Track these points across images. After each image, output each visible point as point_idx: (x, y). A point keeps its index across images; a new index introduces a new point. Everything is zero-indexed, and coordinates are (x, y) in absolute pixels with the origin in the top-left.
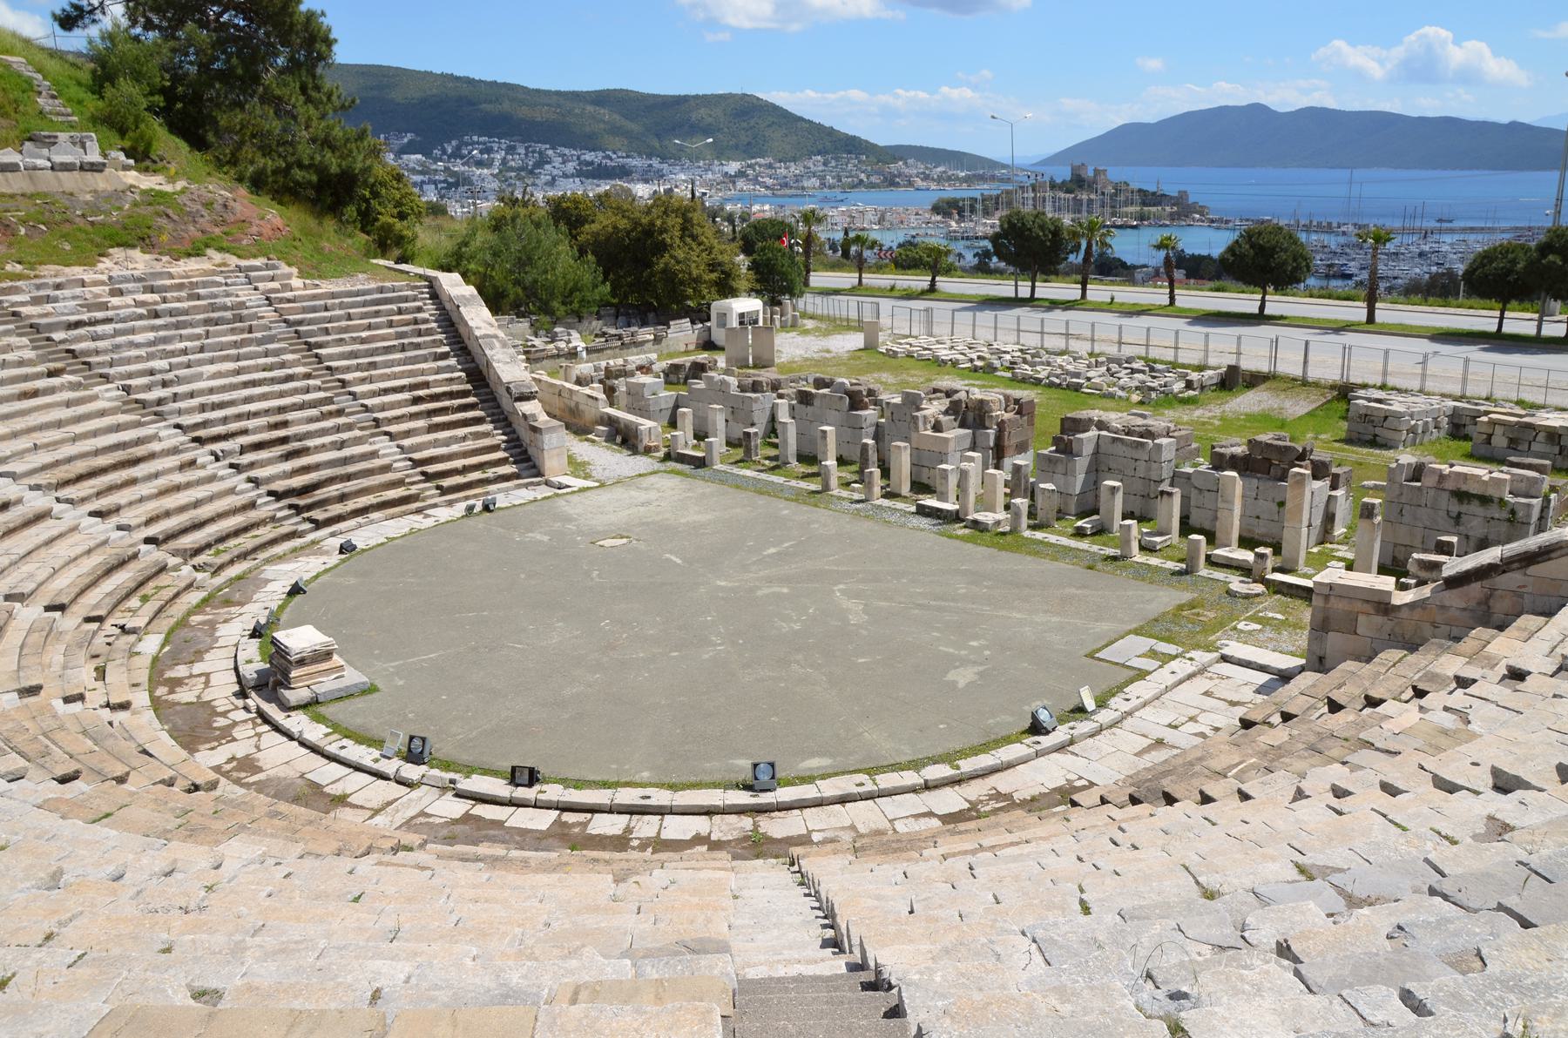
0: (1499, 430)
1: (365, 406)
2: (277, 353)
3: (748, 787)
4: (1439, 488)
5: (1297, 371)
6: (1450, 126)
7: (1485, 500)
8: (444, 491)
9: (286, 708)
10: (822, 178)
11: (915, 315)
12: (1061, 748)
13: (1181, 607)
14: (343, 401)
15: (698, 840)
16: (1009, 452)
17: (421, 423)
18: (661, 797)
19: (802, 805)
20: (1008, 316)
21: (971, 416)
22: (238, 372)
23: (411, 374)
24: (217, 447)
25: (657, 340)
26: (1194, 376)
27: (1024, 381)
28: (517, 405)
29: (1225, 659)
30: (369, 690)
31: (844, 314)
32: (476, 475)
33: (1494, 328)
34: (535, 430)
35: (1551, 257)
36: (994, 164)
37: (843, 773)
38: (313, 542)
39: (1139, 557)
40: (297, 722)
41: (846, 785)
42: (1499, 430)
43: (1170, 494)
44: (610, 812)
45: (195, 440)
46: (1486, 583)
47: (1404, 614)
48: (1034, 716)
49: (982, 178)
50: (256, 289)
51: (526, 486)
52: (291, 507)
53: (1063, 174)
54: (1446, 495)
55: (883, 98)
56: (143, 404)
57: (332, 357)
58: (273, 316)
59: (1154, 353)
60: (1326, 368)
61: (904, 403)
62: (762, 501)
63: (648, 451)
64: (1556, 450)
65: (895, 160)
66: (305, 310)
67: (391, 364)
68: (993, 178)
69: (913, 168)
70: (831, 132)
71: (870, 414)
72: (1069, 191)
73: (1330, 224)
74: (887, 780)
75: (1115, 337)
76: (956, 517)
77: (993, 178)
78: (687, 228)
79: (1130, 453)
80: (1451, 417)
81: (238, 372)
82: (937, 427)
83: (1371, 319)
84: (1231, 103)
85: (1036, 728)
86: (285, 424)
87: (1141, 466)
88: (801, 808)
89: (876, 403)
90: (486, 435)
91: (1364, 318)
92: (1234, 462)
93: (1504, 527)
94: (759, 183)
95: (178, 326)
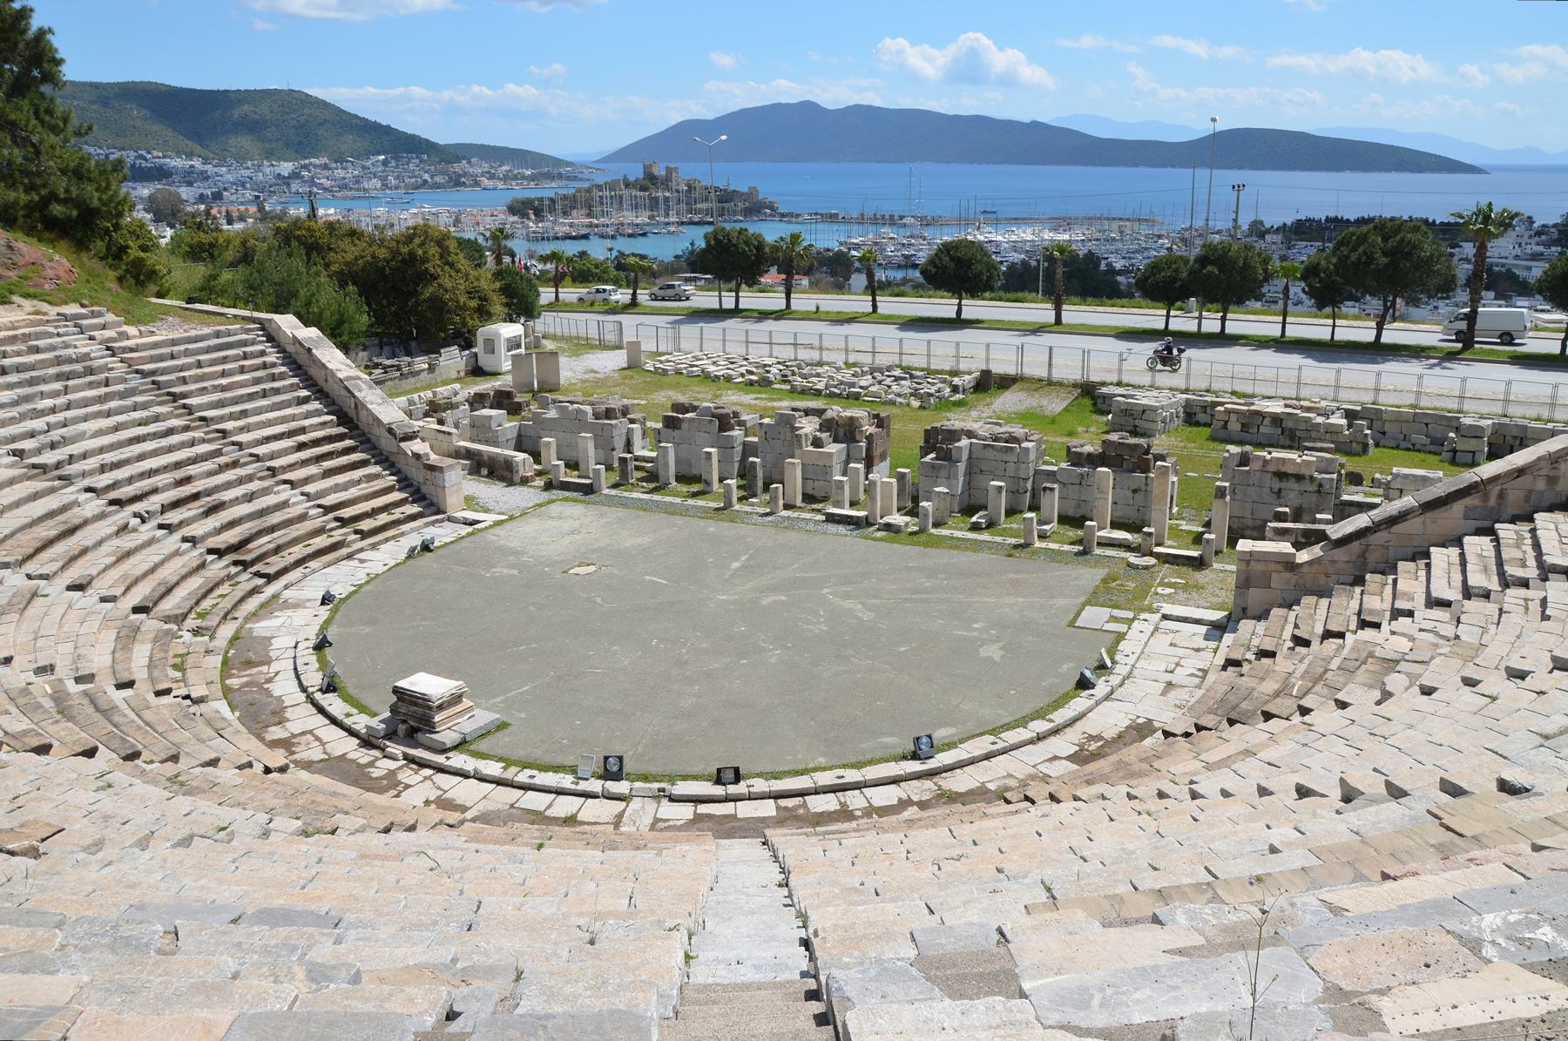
0: (1233, 417)
1: (256, 455)
2: (144, 406)
3: (915, 756)
4: (1263, 471)
5: (1042, 373)
6: (981, 123)
7: (1299, 478)
8: (364, 535)
9: (443, 750)
10: (384, 179)
11: (662, 332)
12: (1108, 697)
13: (1105, 581)
14: (242, 456)
15: (904, 804)
16: (876, 461)
17: (313, 470)
18: (852, 776)
19: (961, 765)
20: (712, 329)
21: (845, 432)
22: (116, 429)
23: (284, 420)
24: (138, 507)
25: (431, 369)
26: (956, 381)
27: (804, 392)
28: (403, 445)
29: (1165, 617)
30: (502, 726)
31: (582, 333)
32: (383, 518)
33: (1218, 330)
34: (432, 468)
35: (1209, 268)
36: (558, 162)
37: (973, 737)
38: (276, 596)
39: (1038, 544)
40: (458, 760)
41: (982, 745)
42: (1233, 417)
43: (1052, 490)
44: (816, 793)
45: (113, 502)
46: (1363, 541)
47: (1305, 569)
48: (1082, 674)
49: (549, 177)
50: (92, 338)
51: (433, 523)
52: (236, 563)
53: (636, 172)
54: (1269, 476)
55: (446, 95)
56: (44, 468)
57: (202, 407)
58: (119, 369)
59: (907, 361)
60: (1068, 369)
61: (777, 424)
62: (680, 521)
63: (525, 481)
64: (1279, 431)
65: (458, 159)
66: (153, 359)
67: (259, 411)
68: (560, 176)
69: (478, 168)
70: (387, 130)
71: (737, 433)
72: (643, 189)
73: (892, 217)
74: (1012, 737)
75: (843, 345)
76: (866, 523)
77: (560, 176)
78: (444, 253)
79: (999, 456)
80: (1185, 407)
81: (116, 429)
82: (817, 443)
83: (1058, 321)
84: (783, 100)
85: (1084, 684)
86: (187, 480)
87: (1011, 468)
88: (961, 767)
89: (742, 424)
90: (377, 476)
91: (1053, 320)
92: (1094, 460)
93: (1314, 498)
94: (316, 185)
95: (32, 382)
